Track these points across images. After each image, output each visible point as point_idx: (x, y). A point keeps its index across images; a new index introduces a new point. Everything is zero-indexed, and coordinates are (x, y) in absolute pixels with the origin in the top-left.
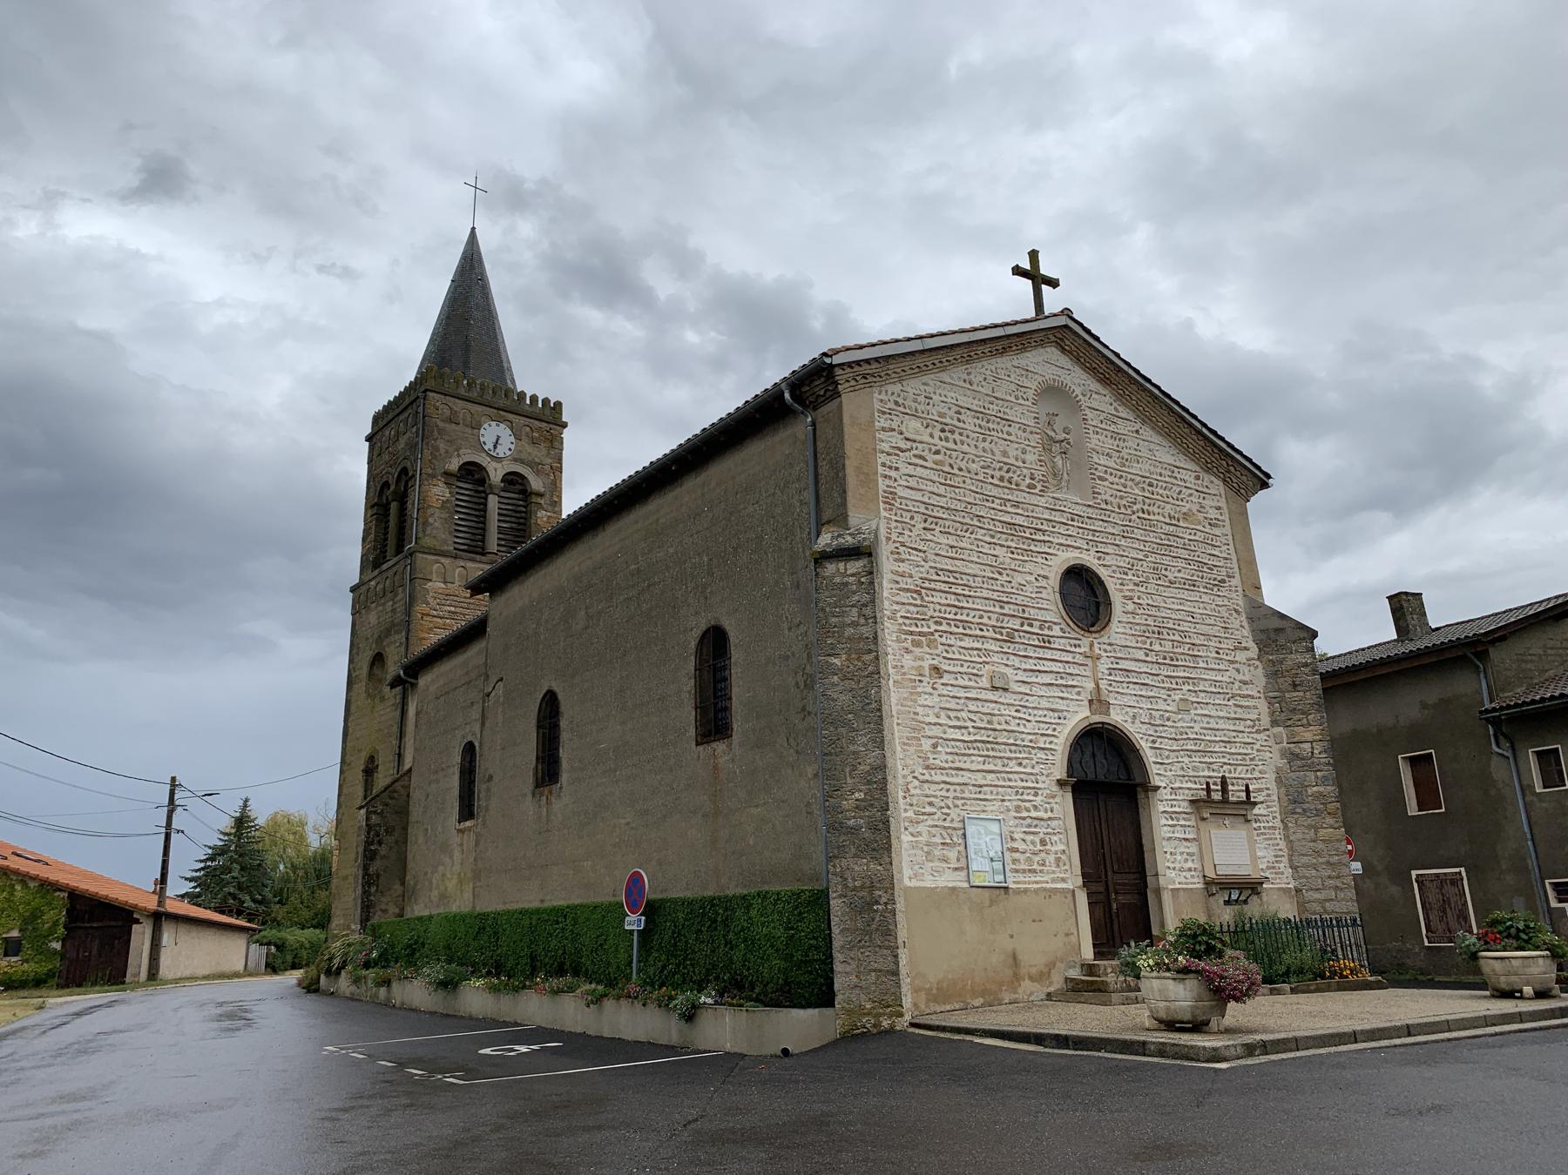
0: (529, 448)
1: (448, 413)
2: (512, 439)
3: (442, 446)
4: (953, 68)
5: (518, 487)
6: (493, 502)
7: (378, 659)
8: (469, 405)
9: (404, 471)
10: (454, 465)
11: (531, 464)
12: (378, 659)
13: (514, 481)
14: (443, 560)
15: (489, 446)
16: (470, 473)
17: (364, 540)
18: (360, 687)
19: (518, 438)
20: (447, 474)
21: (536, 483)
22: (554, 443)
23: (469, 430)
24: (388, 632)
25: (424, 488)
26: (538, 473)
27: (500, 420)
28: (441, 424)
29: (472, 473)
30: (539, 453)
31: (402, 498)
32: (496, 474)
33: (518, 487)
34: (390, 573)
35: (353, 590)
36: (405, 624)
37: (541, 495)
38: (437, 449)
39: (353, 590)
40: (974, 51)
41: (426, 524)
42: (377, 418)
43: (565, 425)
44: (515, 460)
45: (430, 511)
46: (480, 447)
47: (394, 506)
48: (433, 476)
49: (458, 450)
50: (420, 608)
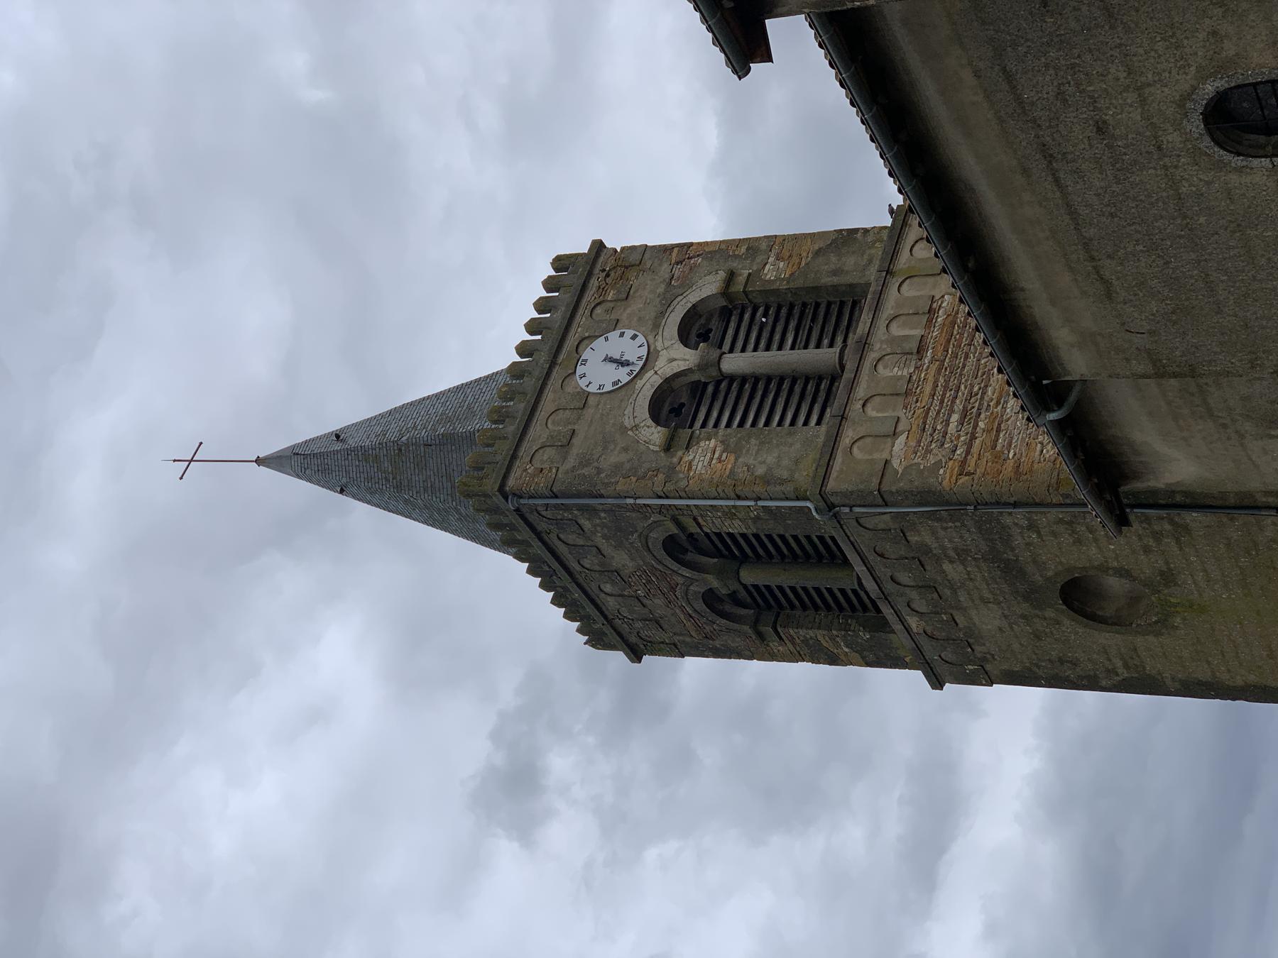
0: (636, 305)
1: (550, 452)
2: (613, 335)
3: (614, 458)
4: (316, 95)
5: (715, 324)
6: (735, 363)
7: (1078, 595)
8: (541, 414)
9: (671, 546)
10: (654, 435)
11: (667, 303)
12: (1078, 595)
13: (694, 329)
14: (846, 440)
15: (623, 375)
16: (677, 411)
17: (833, 660)
18: (785, 9)
19: (616, 324)
20: (668, 447)
21: (707, 287)
22: (633, 262)
23: (589, 412)
24: (1010, 570)
25: (693, 486)
26: (687, 284)
27: (577, 359)
28: (571, 461)
29: (677, 406)
30: (647, 288)
31: (731, 551)
32: (678, 358)
33: (715, 324)
34: (883, 571)
35: (937, 683)
36: (982, 511)
37: (731, 276)
38: (617, 467)
39: (937, 683)
40: (293, 63)
41: (767, 480)
42: (597, 640)
43: (598, 246)
44: (656, 327)
45: (742, 473)
46: (620, 389)
47: (750, 576)
48: (672, 469)
49: (623, 430)
50: (946, 479)
